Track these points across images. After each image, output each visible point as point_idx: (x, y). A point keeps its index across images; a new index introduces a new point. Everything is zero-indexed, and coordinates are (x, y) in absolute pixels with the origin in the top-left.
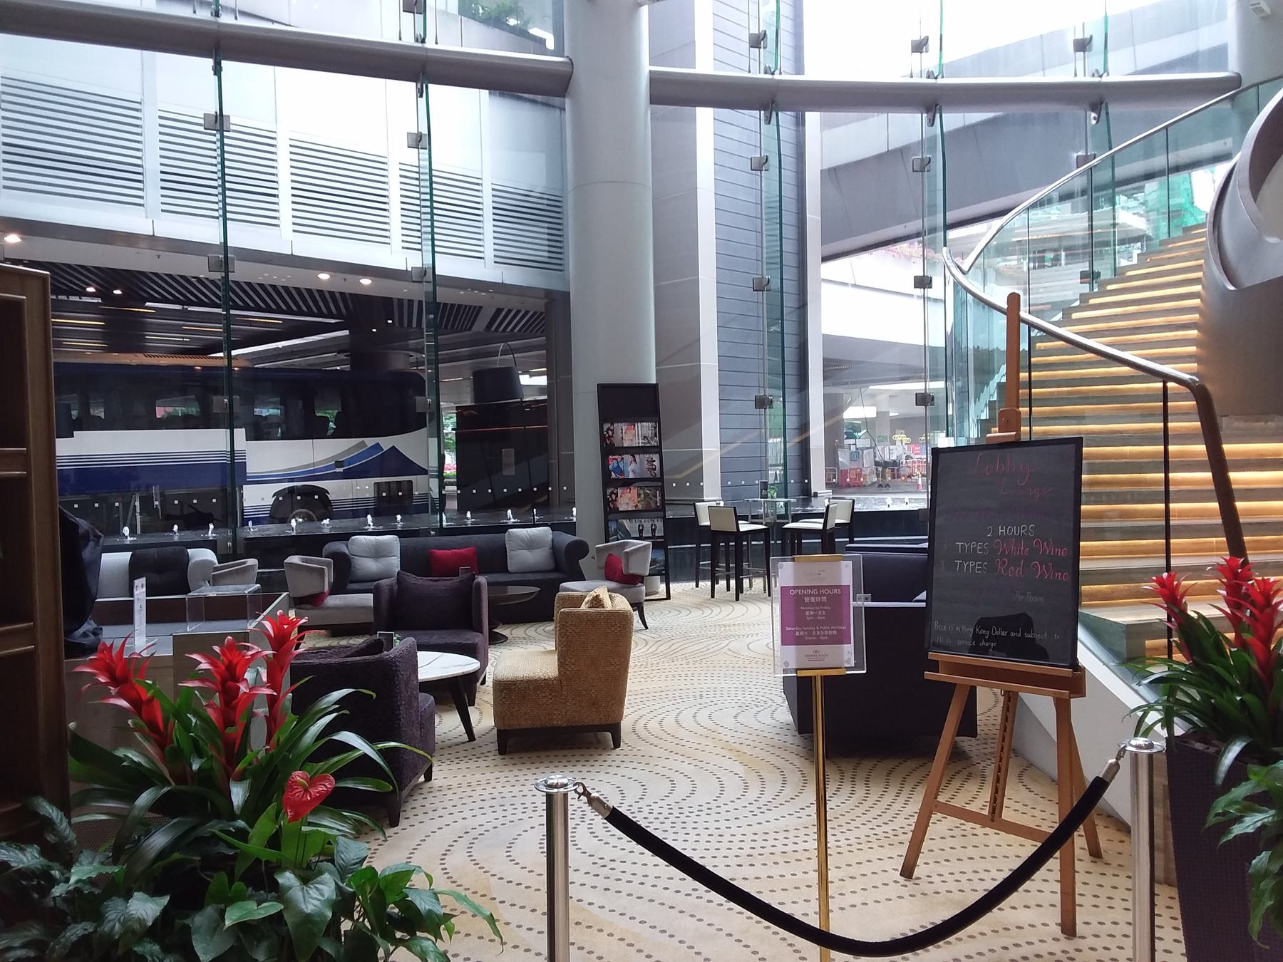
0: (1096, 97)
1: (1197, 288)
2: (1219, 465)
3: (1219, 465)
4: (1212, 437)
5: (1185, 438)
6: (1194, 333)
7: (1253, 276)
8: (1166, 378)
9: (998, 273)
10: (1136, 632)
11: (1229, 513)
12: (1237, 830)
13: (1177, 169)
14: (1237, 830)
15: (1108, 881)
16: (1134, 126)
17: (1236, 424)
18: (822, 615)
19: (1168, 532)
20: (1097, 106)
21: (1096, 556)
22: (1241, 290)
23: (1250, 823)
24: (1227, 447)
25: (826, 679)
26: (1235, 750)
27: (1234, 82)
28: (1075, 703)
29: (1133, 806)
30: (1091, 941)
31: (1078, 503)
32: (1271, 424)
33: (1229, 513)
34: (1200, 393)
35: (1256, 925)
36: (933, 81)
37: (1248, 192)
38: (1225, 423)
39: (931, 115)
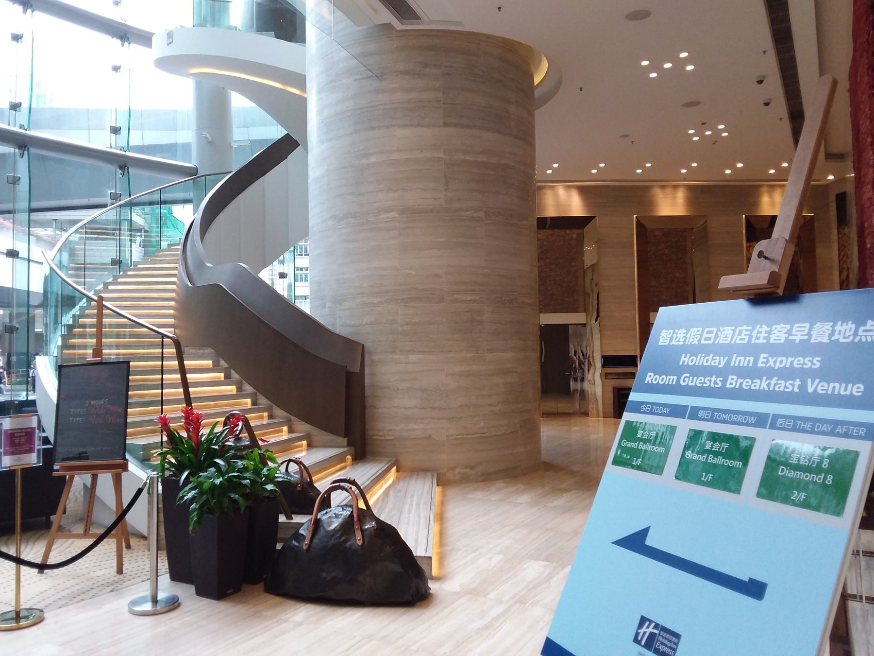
0: (123, 163)
1: (175, 279)
2: (183, 371)
3: (183, 371)
4: (180, 357)
5: (170, 358)
6: (172, 303)
8: (163, 336)
9: (39, 239)
10: (147, 448)
11: (187, 393)
12: (186, 498)
13: (165, 202)
14: (186, 498)
15: (135, 554)
16: (145, 186)
17: (191, 351)
18: (23, 440)
19: (162, 403)
20: (123, 167)
21: (134, 414)
22: (195, 287)
23: (190, 495)
24: (185, 362)
25: (23, 470)
26: (186, 474)
28: (124, 475)
29: (149, 504)
30: (129, 573)
31: (128, 390)
32: (206, 351)
33: (187, 393)
34: (177, 344)
35: (191, 528)
36: (23, 131)
37: (199, 238)
38: (186, 350)
39: (21, 151)
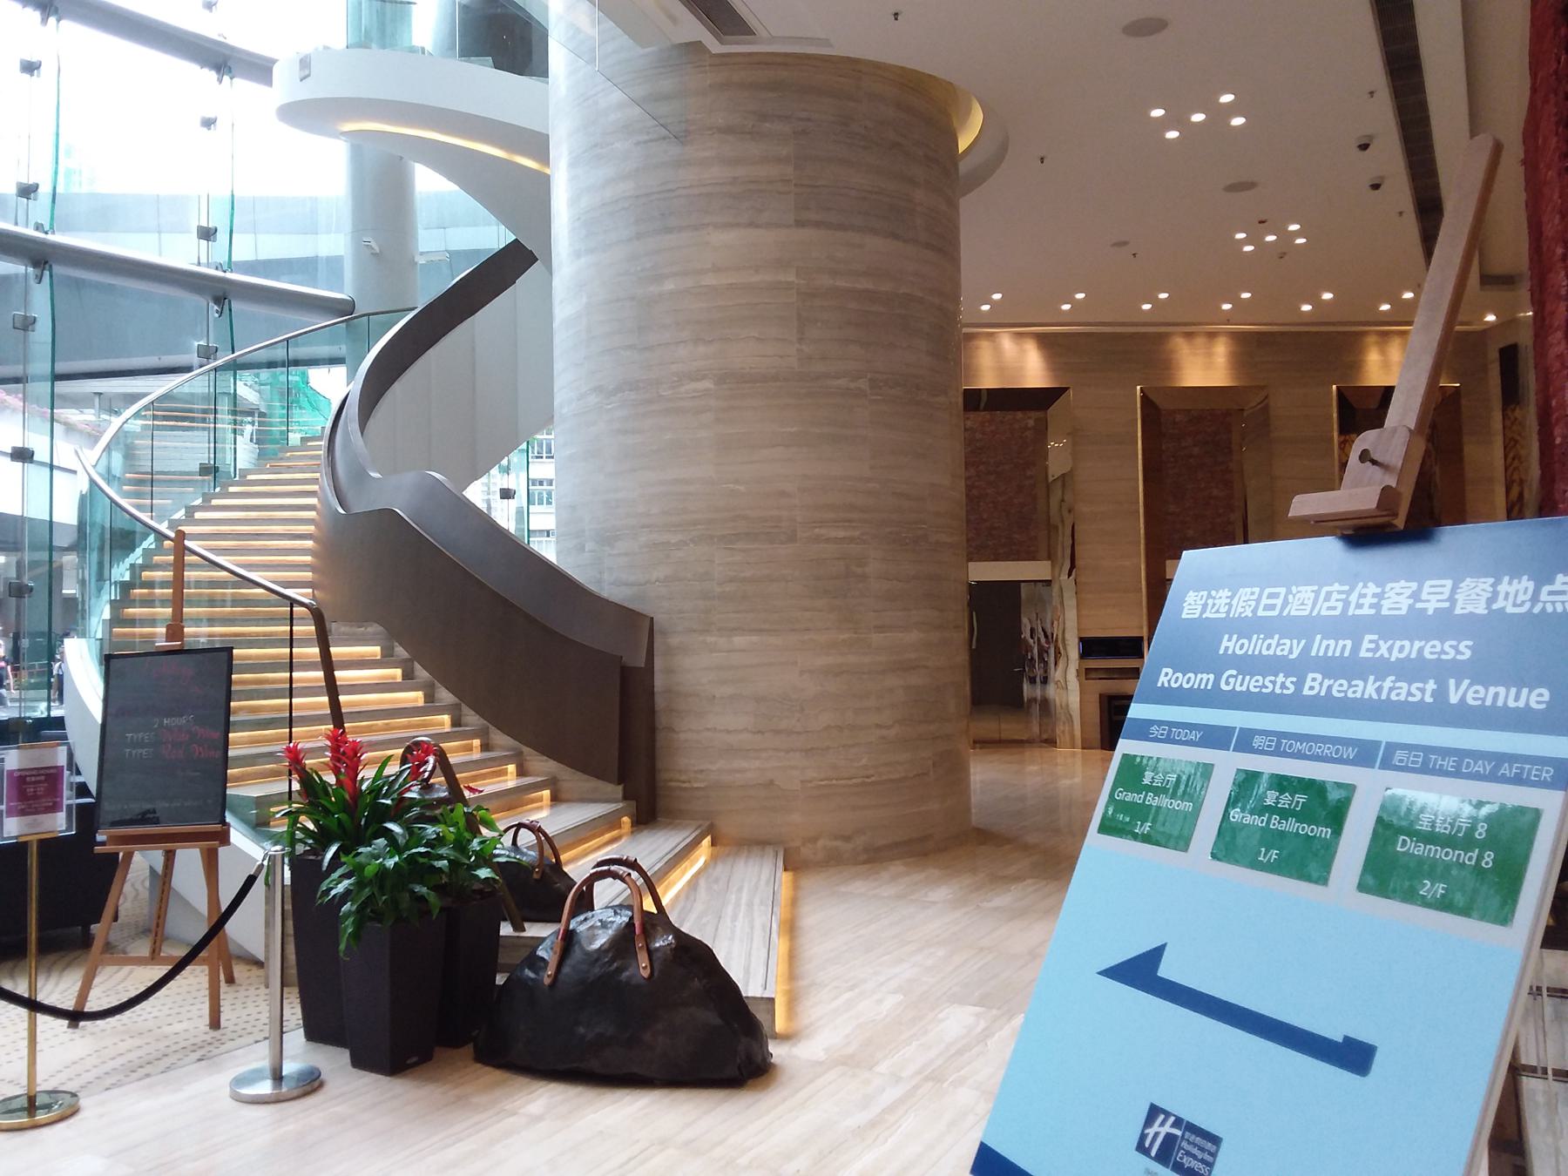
0: (220, 293)
1: (313, 501)
2: (328, 664)
3: (328, 664)
4: (323, 640)
5: (305, 642)
6: (309, 543)
7: (359, 507)
8: (293, 602)
10: (263, 802)
11: (335, 705)
12: (333, 893)
13: (296, 363)
14: (333, 893)
15: (242, 993)
16: (260, 333)
17: (343, 629)
18: (41, 789)
19: (291, 722)
20: (220, 300)
21: (240, 742)
22: (349, 515)
23: (341, 888)
24: (333, 650)
25: (42, 842)
26: (333, 849)
27: (344, 309)
28: (222, 851)
29: (267, 903)
31: (229, 700)
32: (370, 629)
33: (335, 705)
34: (318, 617)
35: (342, 947)
36: (42, 235)
38: (334, 628)
39: (38, 271)
